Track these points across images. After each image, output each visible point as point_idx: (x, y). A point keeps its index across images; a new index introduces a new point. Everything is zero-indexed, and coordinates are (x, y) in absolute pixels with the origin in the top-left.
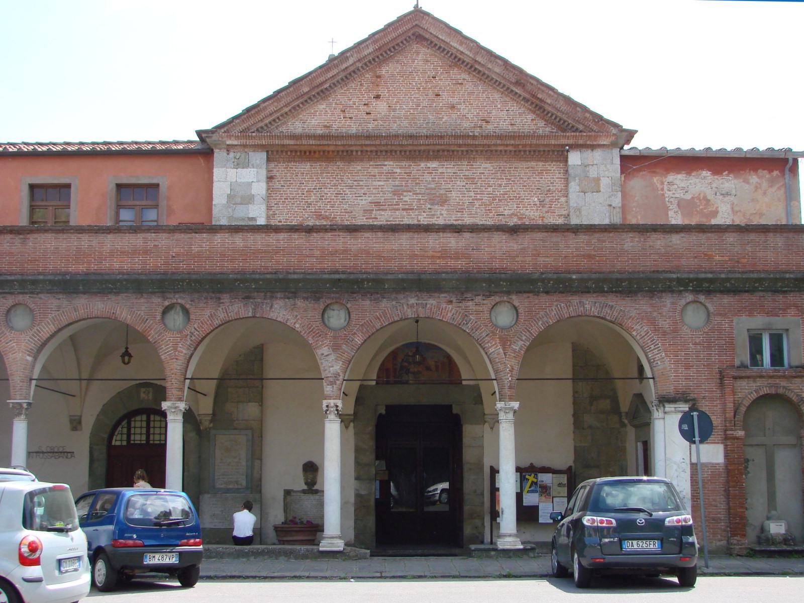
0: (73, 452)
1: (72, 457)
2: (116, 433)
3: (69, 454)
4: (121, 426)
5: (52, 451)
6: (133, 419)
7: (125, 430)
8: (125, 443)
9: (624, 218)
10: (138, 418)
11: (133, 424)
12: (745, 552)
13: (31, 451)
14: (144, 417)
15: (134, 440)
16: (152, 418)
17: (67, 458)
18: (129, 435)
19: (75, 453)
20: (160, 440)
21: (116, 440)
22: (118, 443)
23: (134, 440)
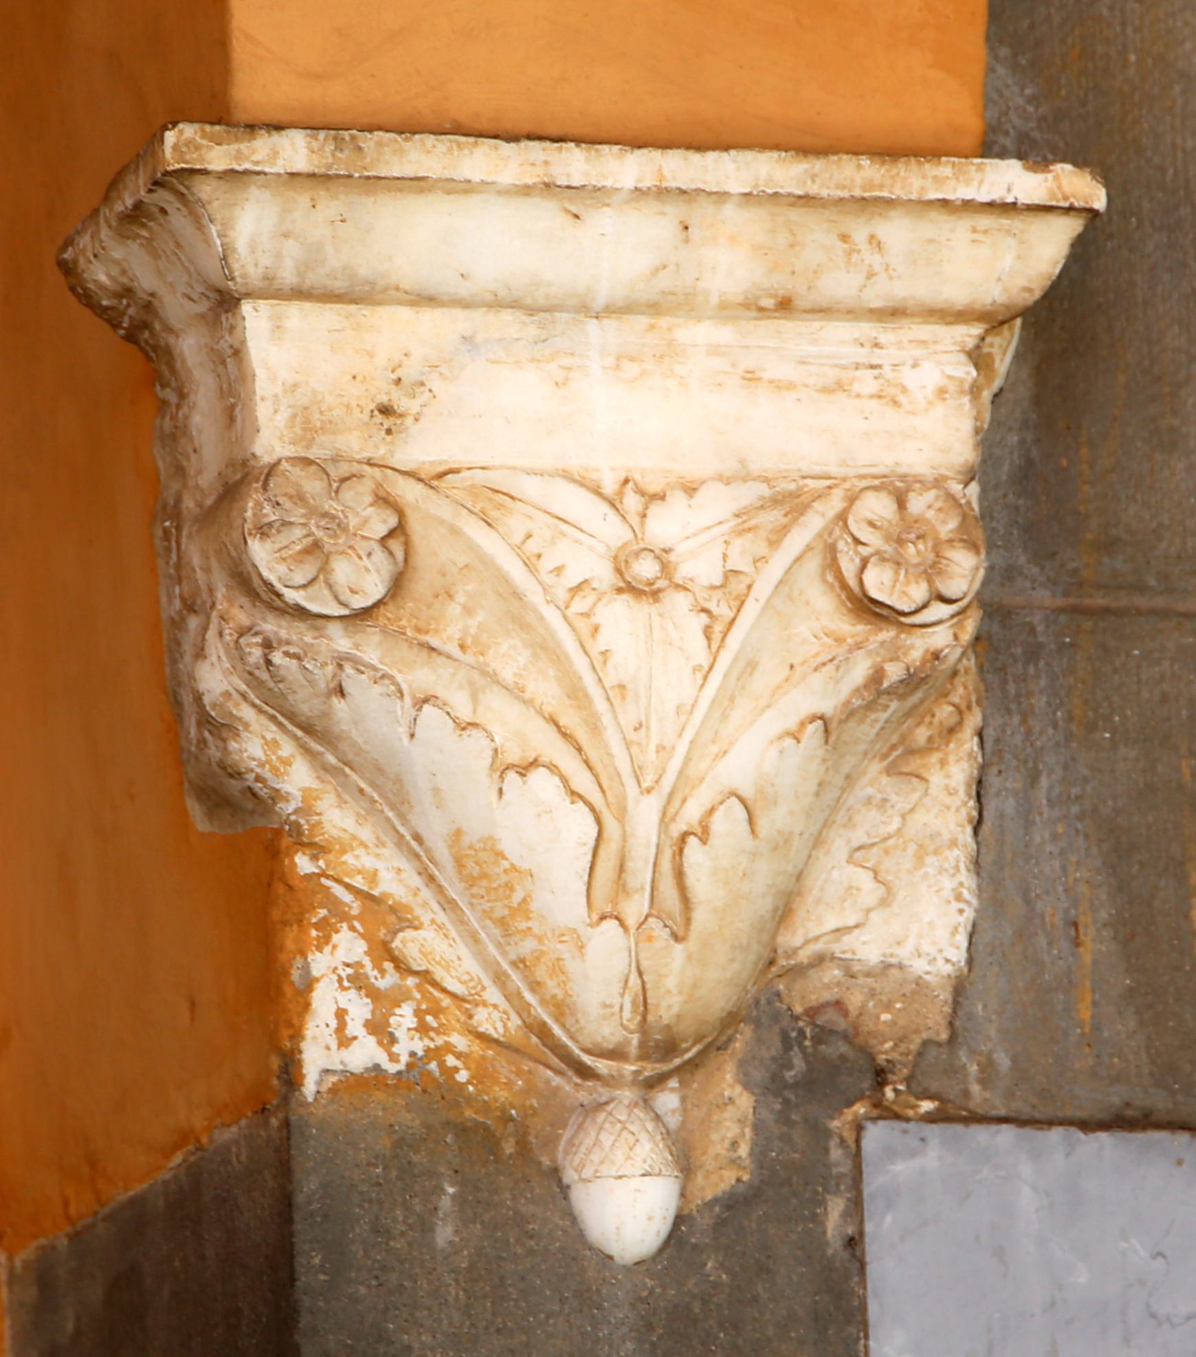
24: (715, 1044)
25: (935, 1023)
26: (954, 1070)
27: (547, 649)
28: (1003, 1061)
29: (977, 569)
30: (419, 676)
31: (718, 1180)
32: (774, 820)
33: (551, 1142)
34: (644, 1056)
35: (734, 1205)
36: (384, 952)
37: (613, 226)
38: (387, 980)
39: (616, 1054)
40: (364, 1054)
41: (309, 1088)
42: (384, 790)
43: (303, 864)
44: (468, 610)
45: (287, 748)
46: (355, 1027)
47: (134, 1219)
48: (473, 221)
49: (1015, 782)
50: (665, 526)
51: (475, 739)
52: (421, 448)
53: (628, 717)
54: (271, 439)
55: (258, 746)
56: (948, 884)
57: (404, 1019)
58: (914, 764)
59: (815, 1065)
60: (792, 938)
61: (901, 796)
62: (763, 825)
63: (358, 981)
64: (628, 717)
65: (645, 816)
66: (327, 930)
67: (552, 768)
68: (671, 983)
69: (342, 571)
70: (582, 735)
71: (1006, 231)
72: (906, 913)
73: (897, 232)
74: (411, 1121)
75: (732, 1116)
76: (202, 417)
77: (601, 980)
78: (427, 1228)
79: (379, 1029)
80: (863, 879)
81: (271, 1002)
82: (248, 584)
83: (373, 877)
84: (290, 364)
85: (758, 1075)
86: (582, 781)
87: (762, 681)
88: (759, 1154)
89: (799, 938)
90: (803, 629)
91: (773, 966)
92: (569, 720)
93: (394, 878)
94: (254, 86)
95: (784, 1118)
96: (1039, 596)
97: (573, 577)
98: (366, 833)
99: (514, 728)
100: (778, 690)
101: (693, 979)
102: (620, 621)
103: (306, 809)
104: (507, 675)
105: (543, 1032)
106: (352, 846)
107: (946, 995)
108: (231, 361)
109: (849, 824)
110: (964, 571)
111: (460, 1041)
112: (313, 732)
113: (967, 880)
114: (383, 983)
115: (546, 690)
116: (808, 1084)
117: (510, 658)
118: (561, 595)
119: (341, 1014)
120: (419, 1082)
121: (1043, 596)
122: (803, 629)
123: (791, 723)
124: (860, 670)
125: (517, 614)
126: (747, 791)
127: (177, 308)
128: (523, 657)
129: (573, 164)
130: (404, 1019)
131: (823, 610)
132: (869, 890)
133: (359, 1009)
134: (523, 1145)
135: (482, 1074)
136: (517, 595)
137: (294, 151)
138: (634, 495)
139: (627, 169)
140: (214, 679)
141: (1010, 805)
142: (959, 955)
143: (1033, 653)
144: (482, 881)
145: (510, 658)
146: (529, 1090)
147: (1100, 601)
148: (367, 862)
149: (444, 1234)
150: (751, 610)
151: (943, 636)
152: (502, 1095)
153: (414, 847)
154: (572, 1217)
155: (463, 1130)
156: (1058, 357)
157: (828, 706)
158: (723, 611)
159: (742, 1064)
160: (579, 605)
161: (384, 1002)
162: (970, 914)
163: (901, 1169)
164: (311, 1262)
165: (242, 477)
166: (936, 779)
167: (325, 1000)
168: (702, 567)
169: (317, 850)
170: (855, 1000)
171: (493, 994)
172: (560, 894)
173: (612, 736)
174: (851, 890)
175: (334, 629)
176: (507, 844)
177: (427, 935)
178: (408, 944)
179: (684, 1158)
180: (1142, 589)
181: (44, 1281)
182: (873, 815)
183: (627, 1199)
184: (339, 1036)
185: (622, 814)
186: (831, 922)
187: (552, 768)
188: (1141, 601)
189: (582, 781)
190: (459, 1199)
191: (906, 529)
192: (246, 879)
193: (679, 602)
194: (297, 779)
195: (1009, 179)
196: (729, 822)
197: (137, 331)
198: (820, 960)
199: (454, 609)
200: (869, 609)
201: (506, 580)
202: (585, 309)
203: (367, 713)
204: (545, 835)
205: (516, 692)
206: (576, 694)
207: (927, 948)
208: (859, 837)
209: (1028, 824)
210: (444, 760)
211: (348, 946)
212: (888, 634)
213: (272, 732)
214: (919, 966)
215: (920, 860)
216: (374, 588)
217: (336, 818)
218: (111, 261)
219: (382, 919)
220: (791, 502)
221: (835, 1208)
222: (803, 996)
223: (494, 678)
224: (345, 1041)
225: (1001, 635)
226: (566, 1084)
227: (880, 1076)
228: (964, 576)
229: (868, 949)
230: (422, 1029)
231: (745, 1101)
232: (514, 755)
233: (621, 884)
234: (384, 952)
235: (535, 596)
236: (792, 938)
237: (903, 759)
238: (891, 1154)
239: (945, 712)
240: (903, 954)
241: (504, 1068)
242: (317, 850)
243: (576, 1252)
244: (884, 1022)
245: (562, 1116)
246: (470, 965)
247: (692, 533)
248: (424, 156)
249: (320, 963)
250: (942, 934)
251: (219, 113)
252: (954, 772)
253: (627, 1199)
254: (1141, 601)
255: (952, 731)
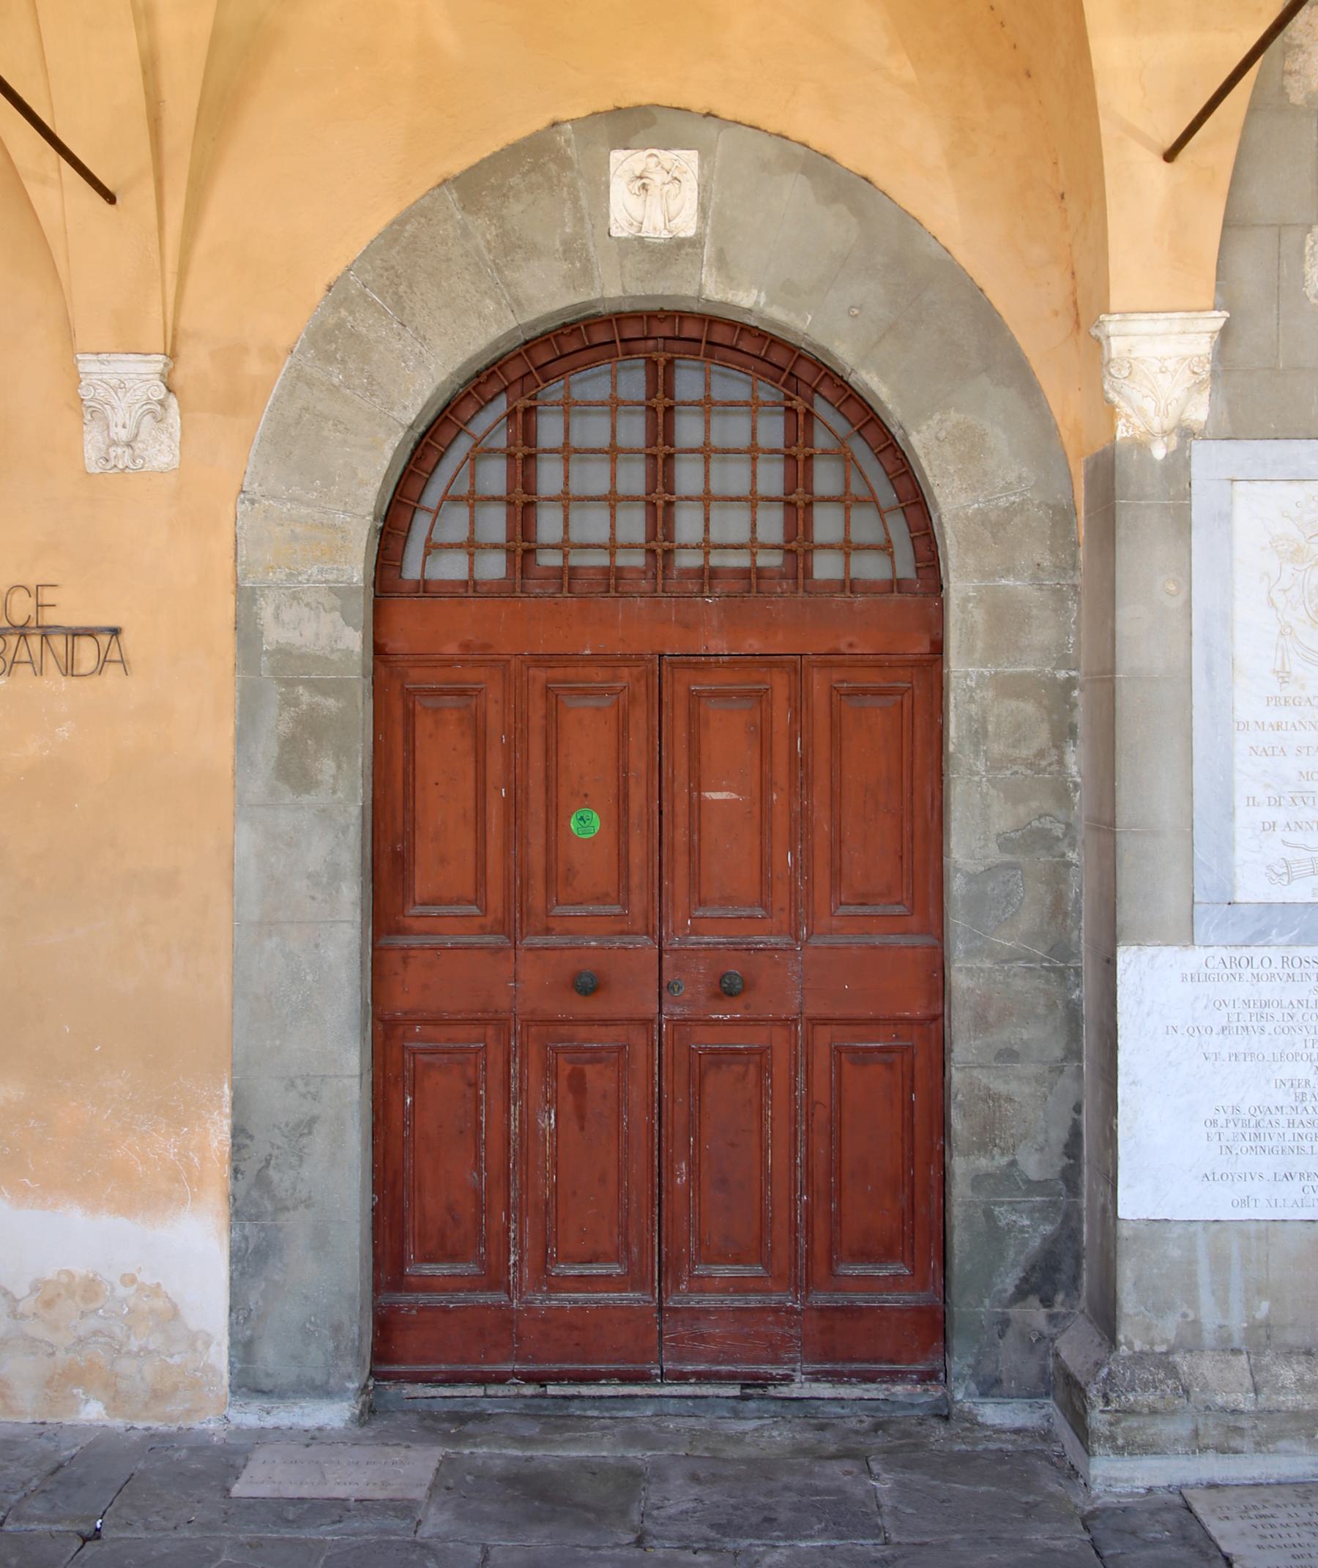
0: (115, 632)
1: (103, 662)
2: (432, 496)
3: (87, 651)
4: (463, 445)
5: (665, 984)
6: (554, 391)
7: (494, 477)
8: (493, 567)
9: (624, 291)
10: (592, 384)
11: (549, 430)
12: (381, 641)
13: (1169, 142)
14: (633, 382)
15: (706, 546)
16: (688, 382)
17: (69, 669)
18: (523, 509)
19: (126, 638)
20: (612, 547)
21: (432, 547)
22: (451, 568)
23: (564, 546)
24: (1172, 431)
29: (624, 368)
31: (1172, 449)
35: (1174, 452)
37: (1160, 323)
40: (1125, 434)
42: (1128, 400)
47: (1097, 455)
48: (1142, 324)
50: (1166, 364)
52: (1133, 355)
54: (1114, 355)
55: (1112, 395)
59: (1186, 434)
71: (1216, 320)
72: (1199, 413)
73: (1200, 322)
75: (1174, 441)
76: (1106, 352)
77: (1156, 425)
81: (1113, 428)
82: (1110, 374)
84: (1117, 346)
89: (1184, 417)
91: (1180, 420)
93: (1129, 411)
94: (1113, 308)
96: (1220, 368)
101: (1169, 423)
102: (1160, 376)
106: (1123, 407)
108: (1109, 344)
110: (1208, 367)
112: (1119, 393)
120: (1133, 438)
127: (1102, 338)
129: (1155, 316)
131: (1188, 372)
137: (1117, 317)
138: (1163, 360)
139: (1163, 316)
140: (1106, 387)
144: (1140, 411)
151: (1205, 376)
156: (1225, 332)
164: (1117, 462)
165: (1110, 360)
167: (1120, 428)
168: (1171, 369)
172: (1151, 413)
179: (1167, 446)
181: (1087, 462)
183: (1159, 452)
184: (1122, 432)
191: (1200, 361)
192: (1110, 411)
195: (1216, 313)
196: (1174, 403)
197: (1098, 340)
200: (1194, 373)
202: (1156, 335)
203: (1126, 390)
204: (1149, 405)
211: (1123, 420)
217: (1122, 404)
218: (1094, 332)
220: (1185, 359)
222: (1184, 424)
225: (1213, 374)
228: (517, 304)
229: (1193, 418)
237: (1199, 392)
243: (1152, 460)
247: (1170, 364)
248: (1135, 316)
251: (1108, 313)
253: (1159, 452)
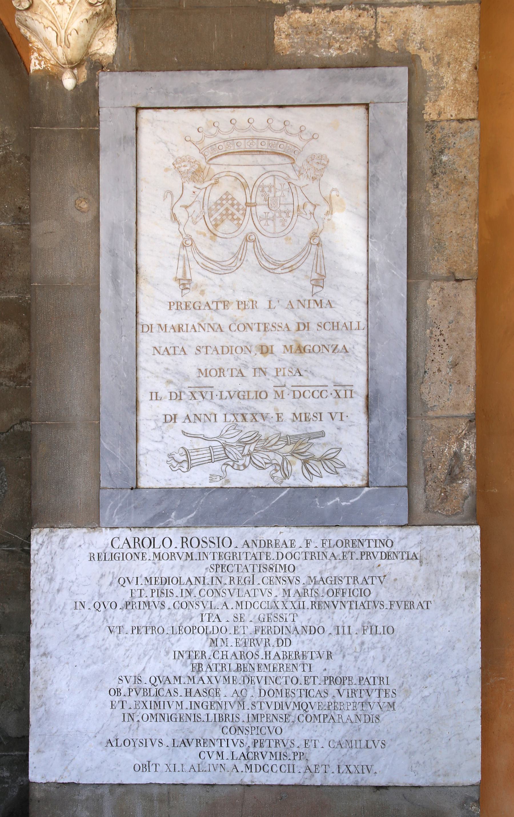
25: (111, 61)
26: (113, 66)
27: (50, 13)
28: (119, 65)
30: (35, 17)
32: (81, 33)
33: (61, 77)
34: (68, 64)
36: (40, 55)
38: (40, 58)
39: (65, 64)
40: (38, 67)
41: (31, 72)
42: (33, 31)
43: (30, 45)
44: (41, 8)
45: (26, 31)
46: (37, 64)
49: (122, 31)
51: (42, 24)
53: (60, 20)
56: (112, 43)
57: (43, 63)
58: (107, 29)
59: (92, 66)
60: (90, 51)
61: (105, 33)
62: (79, 33)
63: (37, 59)
64: (60, 20)
65: (63, 32)
66: (33, 53)
67: (51, 27)
68: (69, 54)
69: (23, 4)
70: (55, 23)
74: (43, 75)
75: (84, 73)
78: (45, 87)
79: (40, 64)
80: (100, 43)
83: (38, 46)
85: (88, 68)
86: (55, 28)
87: (78, 15)
88: (87, 77)
90: (83, 8)
92: (53, 21)
93: (40, 46)
95: (91, 73)
97: (52, 3)
98: (37, 40)
99: (46, 22)
100: (80, 16)
101: (74, 53)
102: (58, 8)
103: (30, 38)
104: (45, 16)
105: (57, 62)
106: (37, 44)
107: (112, 57)
109: (98, 36)
111: (49, 65)
112: (27, 27)
113: (115, 43)
114: (40, 59)
115: (50, 18)
116: (94, 68)
117: (46, 14)
118: (51, 5)
119: (35, 63)
120: (45, 70)
121: (128, 9)
122: (83, 8)
123: (82, 20)
124: (90, 13)
125: (46, 9)
126: (77, 29)
128: (47, 14)
130: (43, 63)
132: (101, 44)
133: (37, 62)
134: (57, 77)
135: (52, 69)
136: (45, 6)
141: (122, 34)
142: (114, 52)
143: (126, 15)
145: (46, 14)
146: (58, 70)
147: (135, 9)
148: (37, 44)
149: (47, 88)
150: (75, 5)
152: (55, 71)
153: (41, 41)
154: (63, 85)
155: (50, 76)
157: (87, 18)
158: (71, 6)
159: (86, 67)
160: (53, 6)
161: (40, 61)
162: (115, 47)
163: (104, 77)
166: (110, 31)
167: (33, 61)
169: (31, 43)
170: (101, 59)
171: (52, 59)
173: (58, 22)
174: (99, 44)
175: (24, 12)
176: (48, 38)
177: (44, 52)
178: (42, 53)
180: (141, 7)
182: (101, 35)
183: (68, 82)
185: (60, 33)
186: (96, 48)
187: (51, 27)
188: (141, 8)
189: (55, 28)
190: (49, 84)
193: (66, 5)
194: (28, 34)
196: (74, 33)
198: (95, 54)
199: (39, 9)
201: (44, 4)
203: (29, 22)
205: (47, 18)
206: (54, 18)
207: (109, 51)
208: (100, 38)
209: (124, 36)
210: (38, 26)
211: (36, 55)
212: (94, 8)
213: (24, 28)
214: (108, 54)
215: (108, 40)
216: (27, 6)
217: (33, 39)
219: (39, 50)
221: (97, 83)
223: (44, 17)
224: (35, 66)
226: (62, 70)
227: (103, 67)
229: (102, 52)
230: (45, 64)
231: (86, 71)
232: (46, 26)
233: (61, 42)
234: (40, 55)
235: (47, 5)
236: (90, 51)
238: (102, 76)
239: (111, 22)
240: (106, 52)
241: (55, 68)
242: (31, 43)
244: (105, 62)
245: (62, 74)
246: (50, 56)
249: (32, 57)
250: (111, 50)
252: (113, 30)
253: (68, 82)
254: (141, 8)
255: (112, 24)
